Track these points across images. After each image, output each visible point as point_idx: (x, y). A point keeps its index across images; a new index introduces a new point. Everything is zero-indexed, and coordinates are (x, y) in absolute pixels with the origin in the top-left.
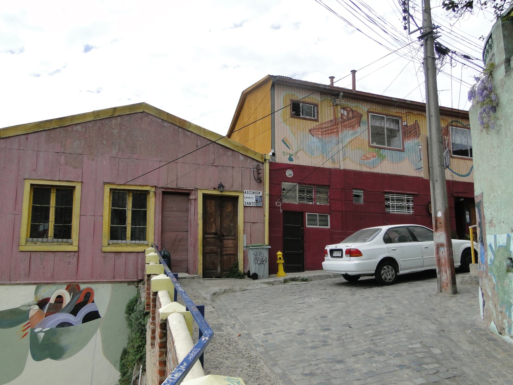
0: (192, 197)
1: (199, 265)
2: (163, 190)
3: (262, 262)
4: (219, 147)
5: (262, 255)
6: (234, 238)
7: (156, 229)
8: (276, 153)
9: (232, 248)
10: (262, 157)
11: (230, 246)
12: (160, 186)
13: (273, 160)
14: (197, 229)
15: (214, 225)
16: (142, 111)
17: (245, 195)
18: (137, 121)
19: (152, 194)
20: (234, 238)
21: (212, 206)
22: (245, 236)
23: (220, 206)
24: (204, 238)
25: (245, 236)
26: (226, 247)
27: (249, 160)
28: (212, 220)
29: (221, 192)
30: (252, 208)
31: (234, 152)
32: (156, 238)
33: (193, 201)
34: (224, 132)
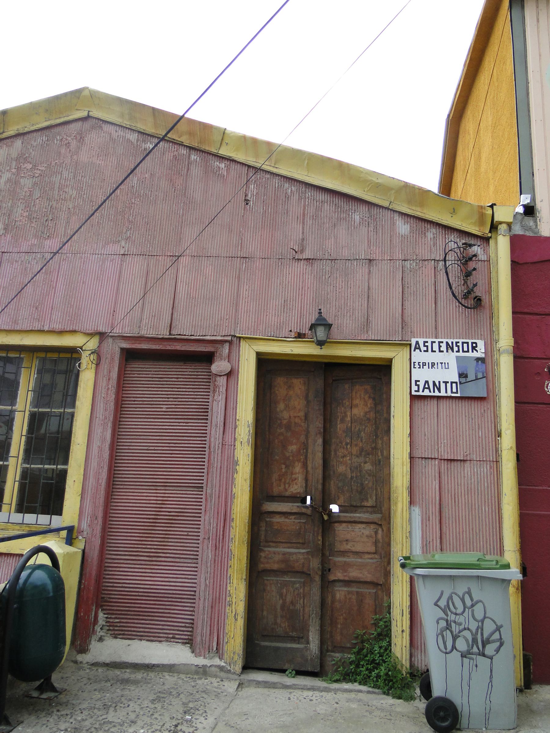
0: (219, 366)
1: (230, 620)
2: (125, 345)
3: (480, 646)
4: (321, 196)
5: (479, 611)
6: (375, 517)
7: (92, 474)
8: (539, 205)
9: (366, 559)
10: (482, 216)
11: (359, 548)
12: (117, 331)
13: (530, 229)
14: (230, 482)
15: (298, 468)
16: (85, 114)
17: (418, 357)
18: (68, 145)
19: (86, 360)
20: (375, 517)
21: (295, 398)
22: (417, 511)
23: (328, 392)
24: (257, 515)
25: (417, 511)
26: (344, 553)
27: (431, 233)
28: (293, 448)
29: (321, 343)
30: (444, 405)
31: (375, 211)
32: (88, 509)
33: (222, 381)
34: (430, 180)
